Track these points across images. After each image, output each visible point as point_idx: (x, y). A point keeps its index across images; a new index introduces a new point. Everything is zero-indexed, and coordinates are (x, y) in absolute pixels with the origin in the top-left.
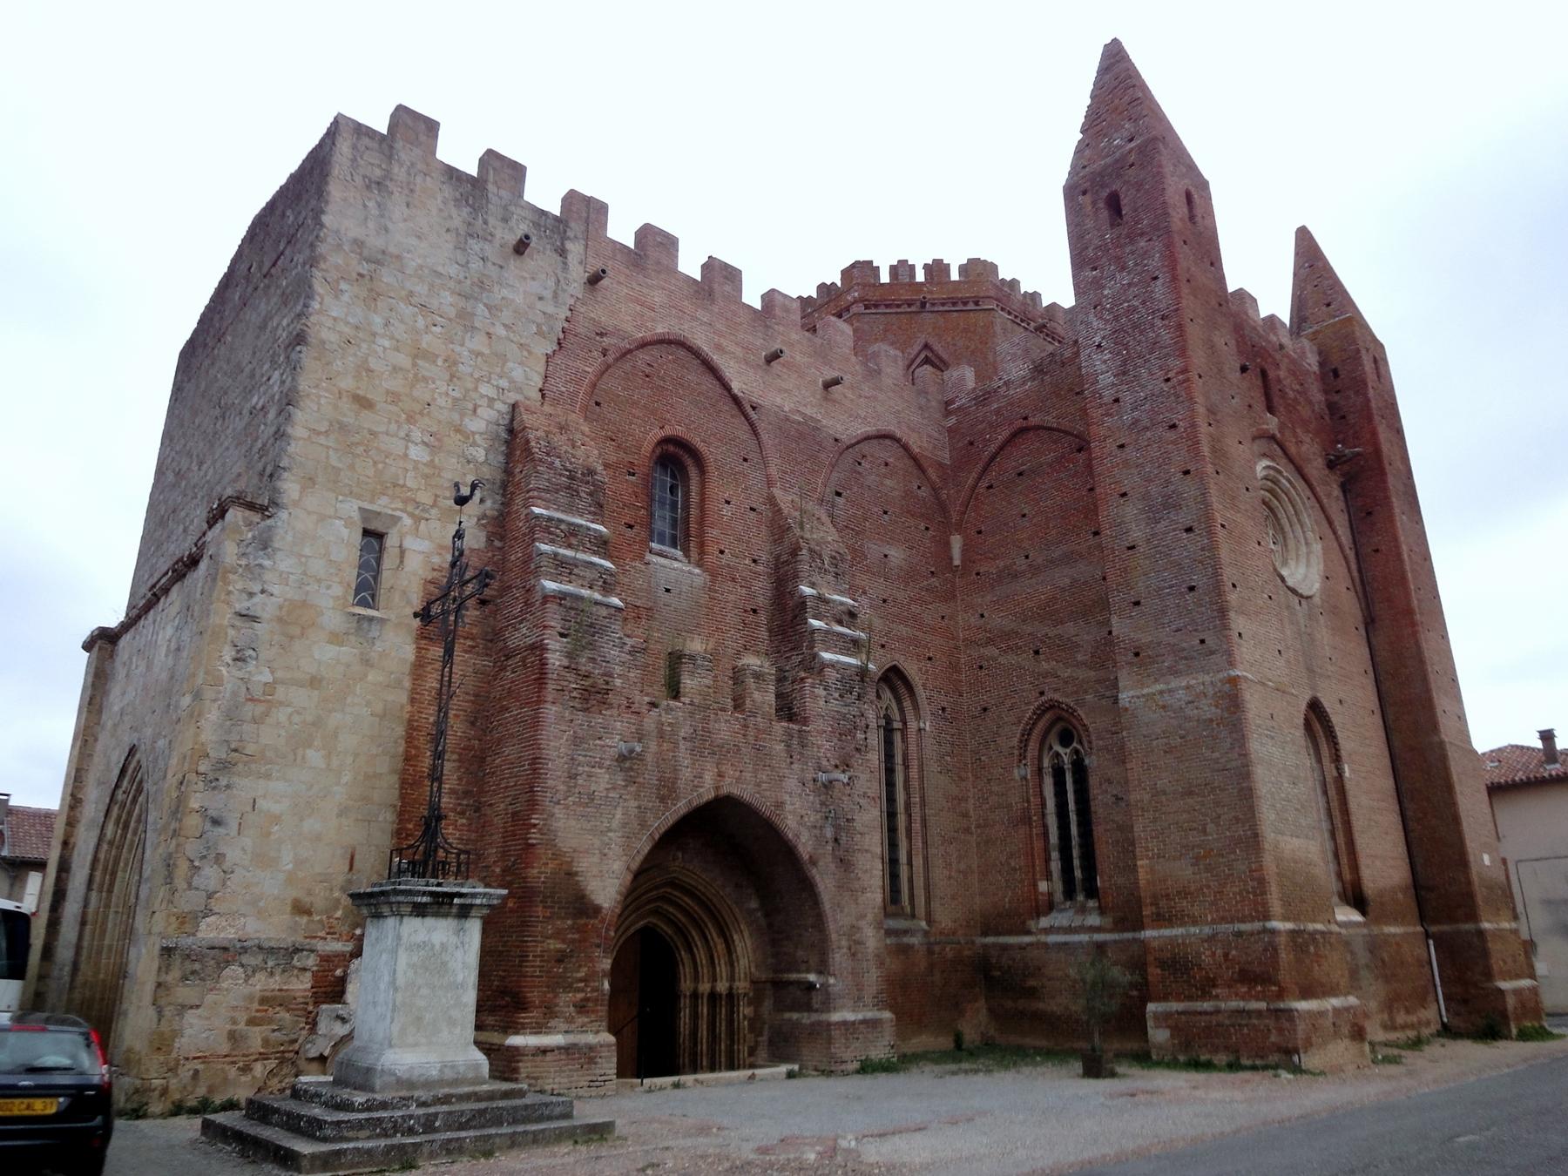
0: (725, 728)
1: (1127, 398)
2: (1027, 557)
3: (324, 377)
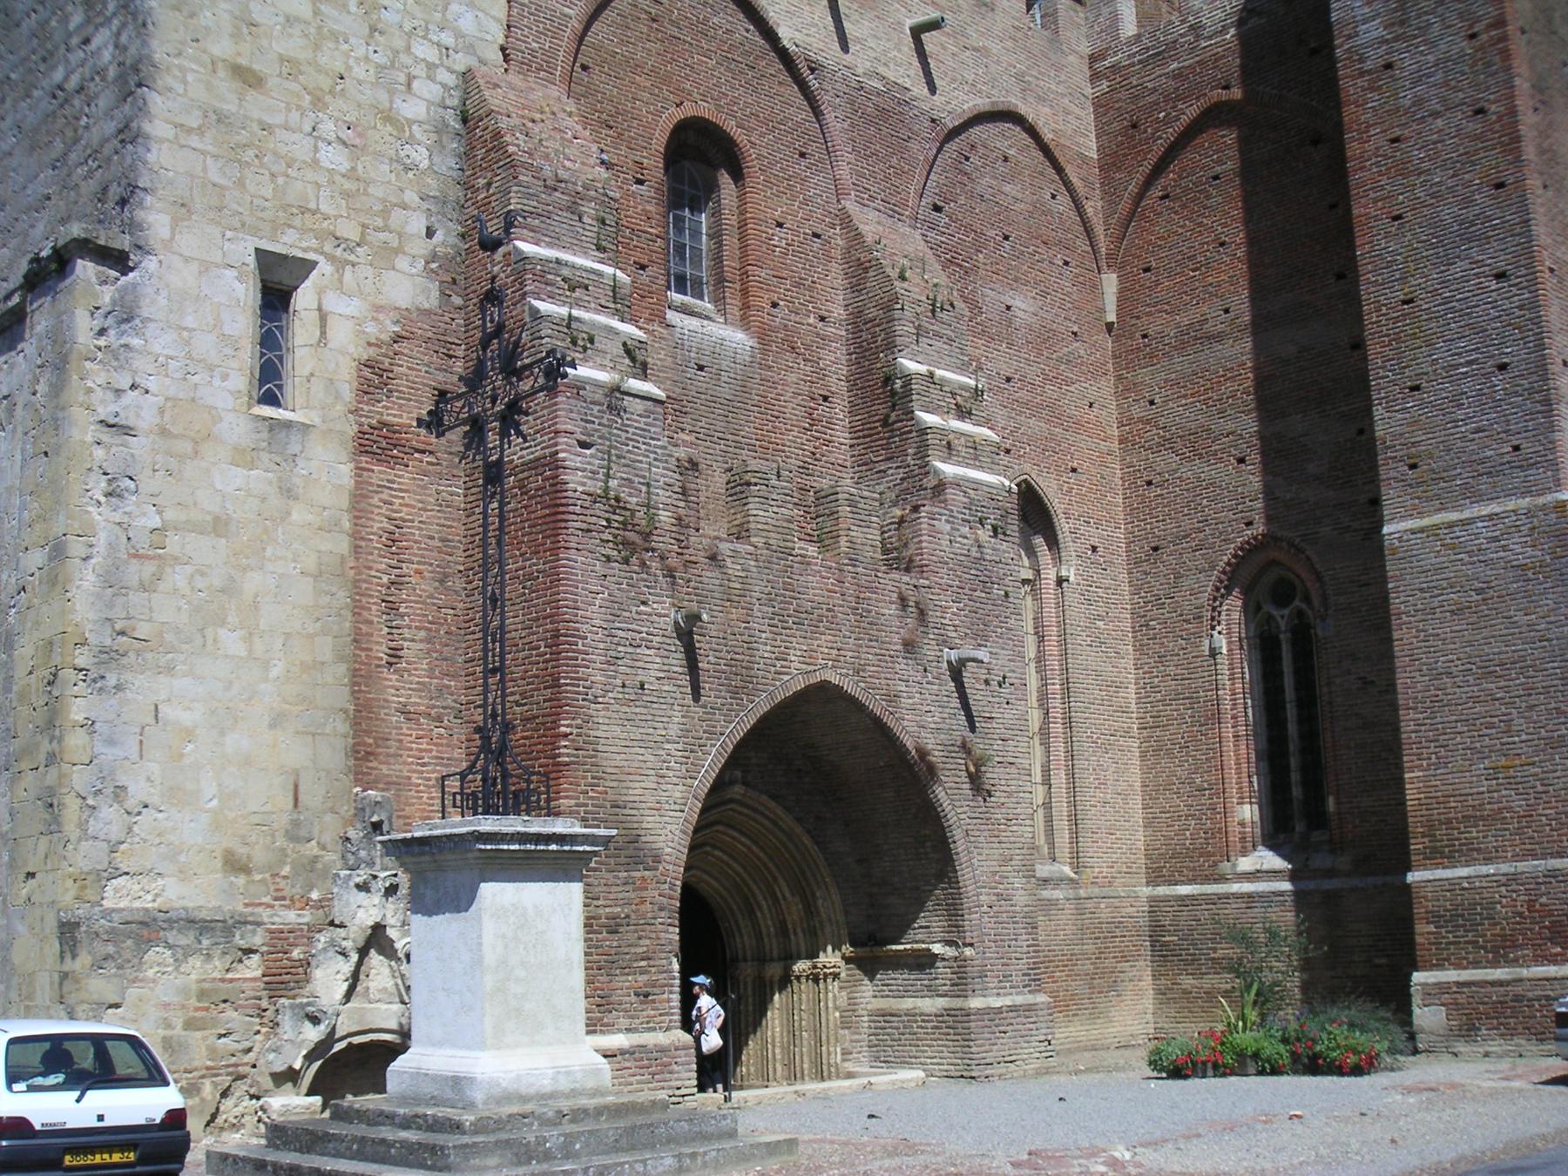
1: (1407, 63)
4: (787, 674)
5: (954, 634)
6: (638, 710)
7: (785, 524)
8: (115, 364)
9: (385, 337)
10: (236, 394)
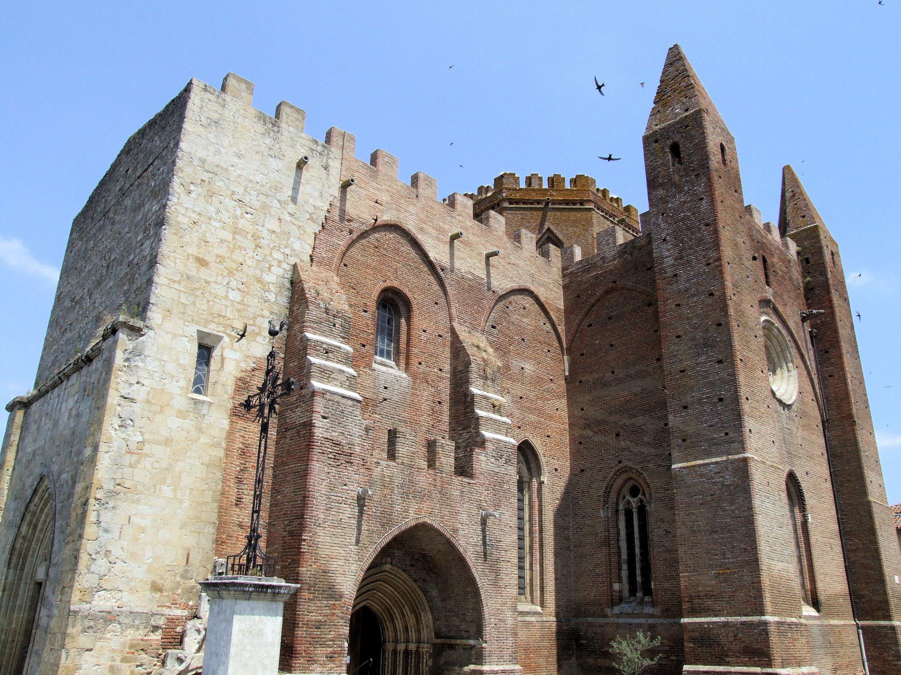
0: (424, 478)
2: (613, 373)
3: (179, 246)
4: (407, 518)
5: (485, 504)
6: (338, 531)
7: (411, 455)
8: (131, 373)
9: (249, 368)
10: (182, 388)
